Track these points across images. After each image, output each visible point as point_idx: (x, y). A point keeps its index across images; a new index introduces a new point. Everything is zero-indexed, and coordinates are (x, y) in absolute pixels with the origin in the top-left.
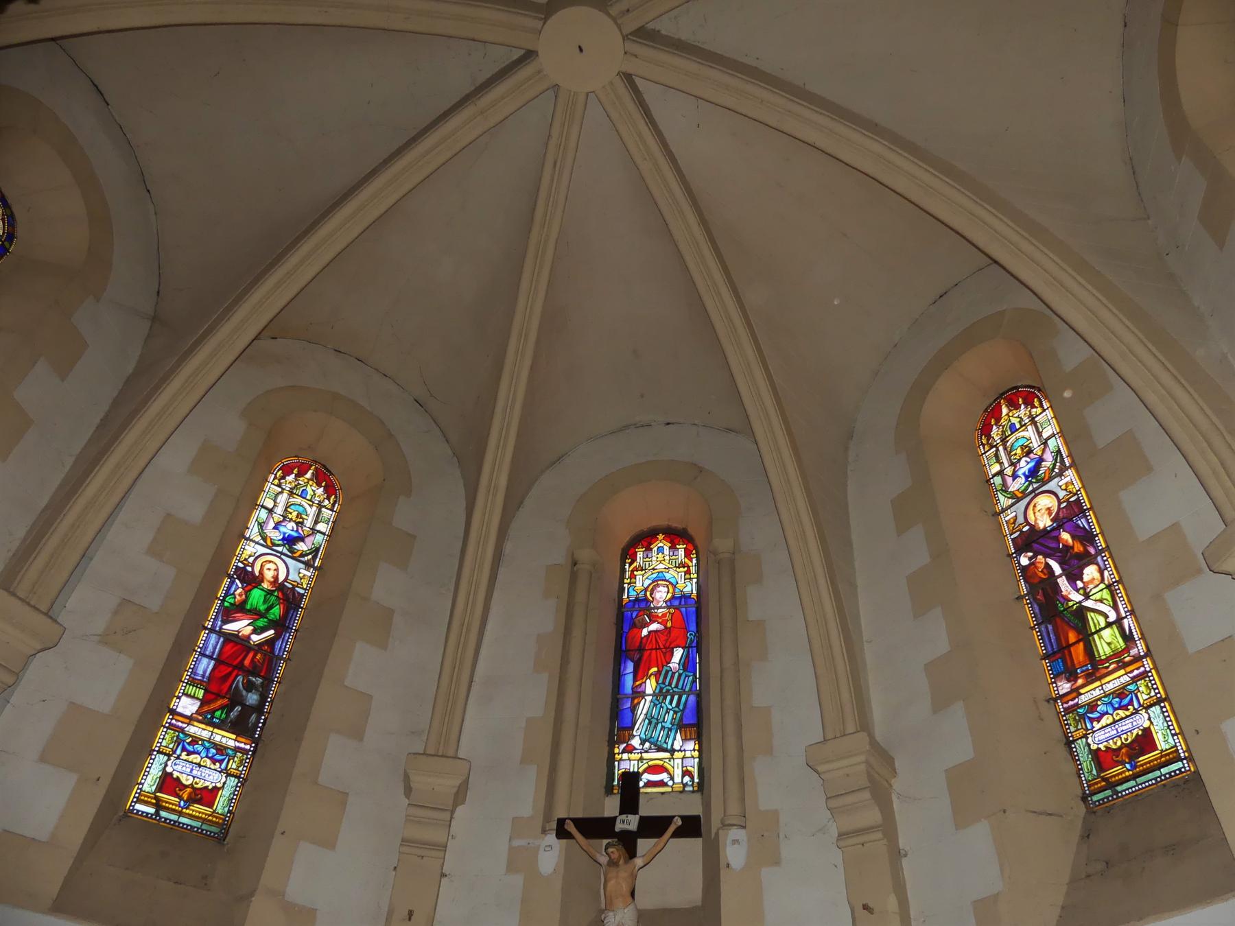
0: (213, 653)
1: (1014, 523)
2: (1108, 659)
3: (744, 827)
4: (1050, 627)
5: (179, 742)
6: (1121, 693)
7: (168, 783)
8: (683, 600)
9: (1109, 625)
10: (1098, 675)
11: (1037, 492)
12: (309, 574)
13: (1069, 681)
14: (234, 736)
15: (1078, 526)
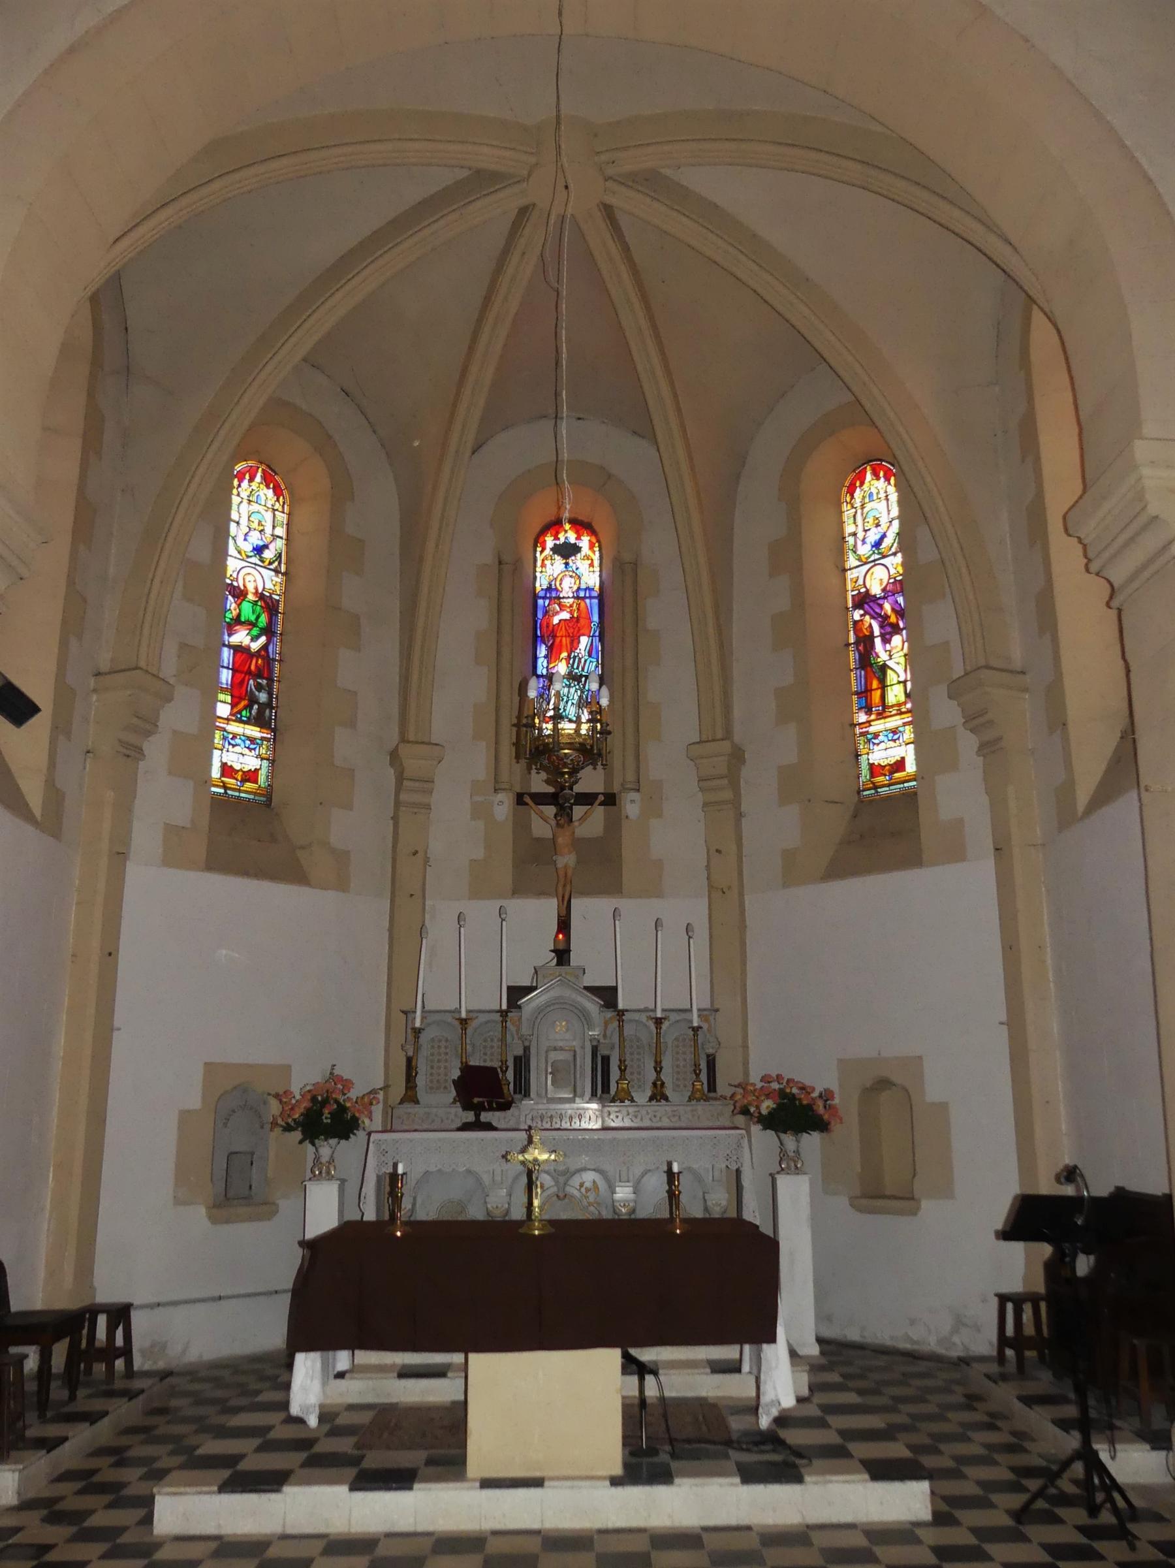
0: (229, 663)
1: (856, 582)
2: (892, 706)
3: (638, 790)
4: (863, 672)
5: (225, 738)
6: (894, 731)
7: (227, 770)
8: (587, 592)
9: (899, 682)
10: (884, 715)
11: (877, 562)
12: (279, 580)
13: (866, 713)
14: (258, 729)
15: (897, 602)
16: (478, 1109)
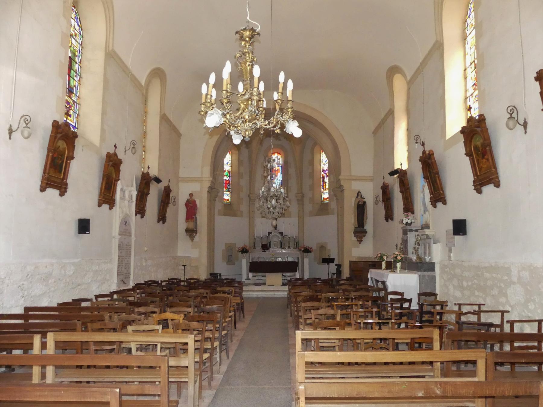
16: (264, 250)
